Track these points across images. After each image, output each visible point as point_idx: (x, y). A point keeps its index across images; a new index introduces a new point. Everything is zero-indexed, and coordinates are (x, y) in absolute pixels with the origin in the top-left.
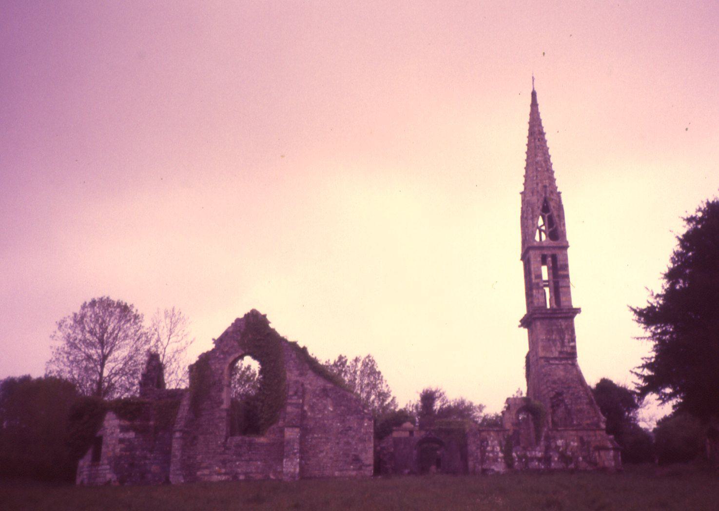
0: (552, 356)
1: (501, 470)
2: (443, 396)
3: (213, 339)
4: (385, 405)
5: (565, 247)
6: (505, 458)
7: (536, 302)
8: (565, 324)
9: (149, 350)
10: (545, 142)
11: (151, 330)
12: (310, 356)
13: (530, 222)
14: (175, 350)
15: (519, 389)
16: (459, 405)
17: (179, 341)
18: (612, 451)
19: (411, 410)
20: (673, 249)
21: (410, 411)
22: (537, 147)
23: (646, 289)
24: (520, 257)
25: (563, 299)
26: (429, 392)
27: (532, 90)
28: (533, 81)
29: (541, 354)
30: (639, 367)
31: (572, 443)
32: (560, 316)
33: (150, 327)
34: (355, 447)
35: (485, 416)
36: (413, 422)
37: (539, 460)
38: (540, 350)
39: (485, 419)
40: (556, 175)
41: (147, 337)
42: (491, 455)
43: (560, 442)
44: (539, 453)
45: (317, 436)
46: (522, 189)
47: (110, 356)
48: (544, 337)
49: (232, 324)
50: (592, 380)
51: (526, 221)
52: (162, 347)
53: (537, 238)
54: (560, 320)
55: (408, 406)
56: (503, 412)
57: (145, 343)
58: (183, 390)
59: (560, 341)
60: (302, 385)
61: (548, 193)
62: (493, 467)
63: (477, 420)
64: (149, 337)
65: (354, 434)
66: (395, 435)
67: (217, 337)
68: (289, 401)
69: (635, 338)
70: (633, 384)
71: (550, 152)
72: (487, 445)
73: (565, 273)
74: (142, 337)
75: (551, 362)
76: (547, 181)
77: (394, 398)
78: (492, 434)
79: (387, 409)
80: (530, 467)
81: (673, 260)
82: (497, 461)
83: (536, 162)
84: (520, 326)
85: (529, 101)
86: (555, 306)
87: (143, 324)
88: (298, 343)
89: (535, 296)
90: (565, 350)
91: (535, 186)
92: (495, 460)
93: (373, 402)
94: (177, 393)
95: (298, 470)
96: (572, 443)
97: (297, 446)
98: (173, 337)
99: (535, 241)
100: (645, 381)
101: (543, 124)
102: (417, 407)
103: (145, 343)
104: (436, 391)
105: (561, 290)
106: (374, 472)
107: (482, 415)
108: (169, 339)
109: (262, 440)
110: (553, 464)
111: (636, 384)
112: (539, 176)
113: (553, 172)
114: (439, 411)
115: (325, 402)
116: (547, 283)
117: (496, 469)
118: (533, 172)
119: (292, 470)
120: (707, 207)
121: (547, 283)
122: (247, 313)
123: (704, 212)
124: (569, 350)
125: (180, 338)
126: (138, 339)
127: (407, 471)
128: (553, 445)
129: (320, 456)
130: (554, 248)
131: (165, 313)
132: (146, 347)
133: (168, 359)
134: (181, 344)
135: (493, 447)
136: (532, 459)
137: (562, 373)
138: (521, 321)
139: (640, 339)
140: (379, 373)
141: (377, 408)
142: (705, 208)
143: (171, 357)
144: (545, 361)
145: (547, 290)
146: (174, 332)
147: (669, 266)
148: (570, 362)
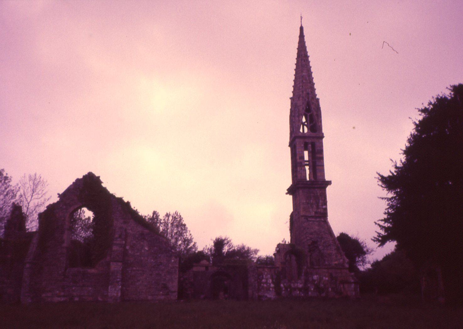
0: (310, 215)
1: (272, 296)
2: (230, 243)
3: (58, 194)
4: (188, 248)
5: (322, 137)
6: (275, 288)
7: (299, 176)
8: (319, 192)
9: (13, 203)
10: (309, 62)
11: (16, 188)
12: (132, 209)
13: (297, 118)
14: (36, 204)
15: (284, 239)
16: (240, 249)
17: (39, 198)
18: (353, 284)
19: (207, 252)
20: (411, 132)
21: (206, 253)
22: (303, 66)
23: (391, 161)
24: (288, 144)
25: (319, 174)
26: (220, 240)
27: (300, 26)
28: (301, 19)
29: (302, 213)
30: (382, 220)
31: (324, 278)
32: (316, 186)
33: (15, 186)
34: (164, 278)
35: (259, 258)
36: (208, 260)
37: (300, 290)
38: (301, 210)
39: (259, 260)
40: (315, 86)
41: (13, 193)
42: (265, 285)
43: (315, 277)
44: (300, 285)
45: (135, 269)
46: (291, 95)
47: (27, 222)
48: (305, 202)
49: (73, 183)
50: (336, 234)
51: (294, 118)
52: (26, 202)
53: (301, 130)
54: (316, 190)
55: (205, 250)
56: (274, 254)
57: (12, 198)
58: (34, 232)
59: (316, 204)
60: (126, 230)
61: (310, 98)
62: (266, 294)
63: (254, 260)
64: (15, 193)
65: (163, 268)
66: (195, 269)
67: (61, 192)
68: (115, 242)
69: (380, 198)
70: (376, 233)
71: (312, 70)
72: (263, 278)
73: (321, 156)
74: (10, 193)
75: (309, 219)
76: (309, 90)
77: (195, 243)
78: (266, 270)
79: (190, 251)
80: (293, 294)
81: (409, 141)
82: (269, 290)
83: (302, 76)
84: (287, 194)
85: (297, 40)
86: (313, 179)
87: (11, 184)
88: (123, 199)
89: (299, 172)
90: (319, 211)
91: (301, 93)
92: (268, 289)
93: (180, 245)
94: (32, 234)
95: (119, 294)
96: (324, 278)
97: (119, 276)
98: (35, 195)
99: (300, 132)
100: (386, 231)
101: (308, 50)
102: (211, 250)
103: (12, 198)
104: (225, 240)
105: (317, 168)
106: (178, 297)
107: (257, 256)
108: (32, 196)
109: (93, 271)
110: (310, 293)
111: (378, 233)
112: (304, 87)
113: (314, 84)
114: (226, 253)
115: (142, 243)
116: (308, 163)
117: (268, 296)
118: (299, 83)
119: (115, 294)
120: (437, 101)
121: (308, 163)
122: (85, 175)
123: (434, 105)
124: (322, 211)
125: (40, 196)
126: (7, 194)
127: (202, 296)
128: (310, 279)
129: (137, 284)
130: (313, 137)
131: (29, 177)
132: (13, 201)
133: (31, 211)
134: (41, 200)
135: (267, 279)
136: (295, 289)
137: (317, 228)
138: (288, 190)
139: (384, 199)
140: (185, 225)
141: (183, 250)
142: (435, 102)
143: (33, 209)
144: (304, 219)
145: (307, 168)
146: (36, 191)
147: (407, 145)
148: (322, 220)
